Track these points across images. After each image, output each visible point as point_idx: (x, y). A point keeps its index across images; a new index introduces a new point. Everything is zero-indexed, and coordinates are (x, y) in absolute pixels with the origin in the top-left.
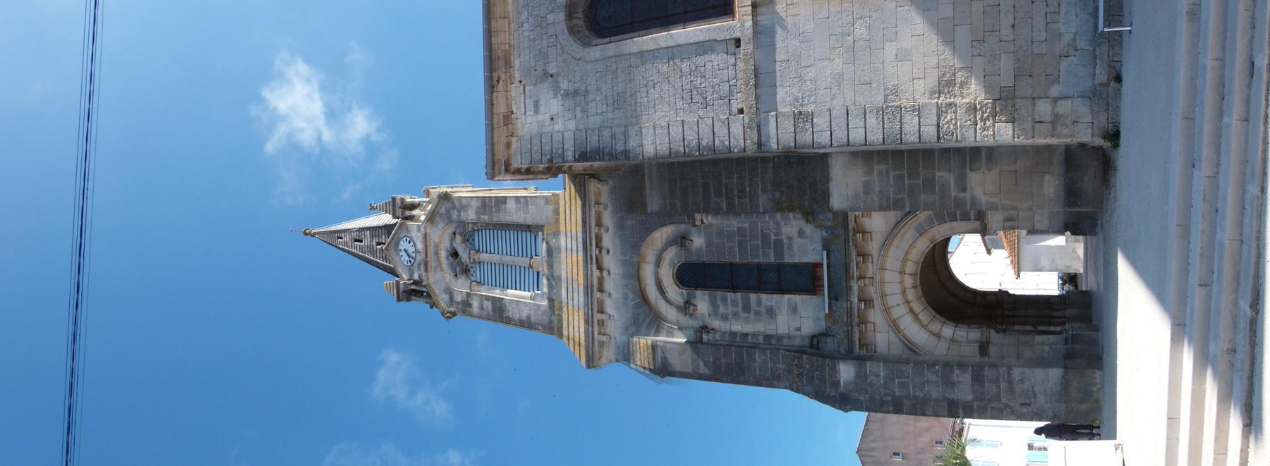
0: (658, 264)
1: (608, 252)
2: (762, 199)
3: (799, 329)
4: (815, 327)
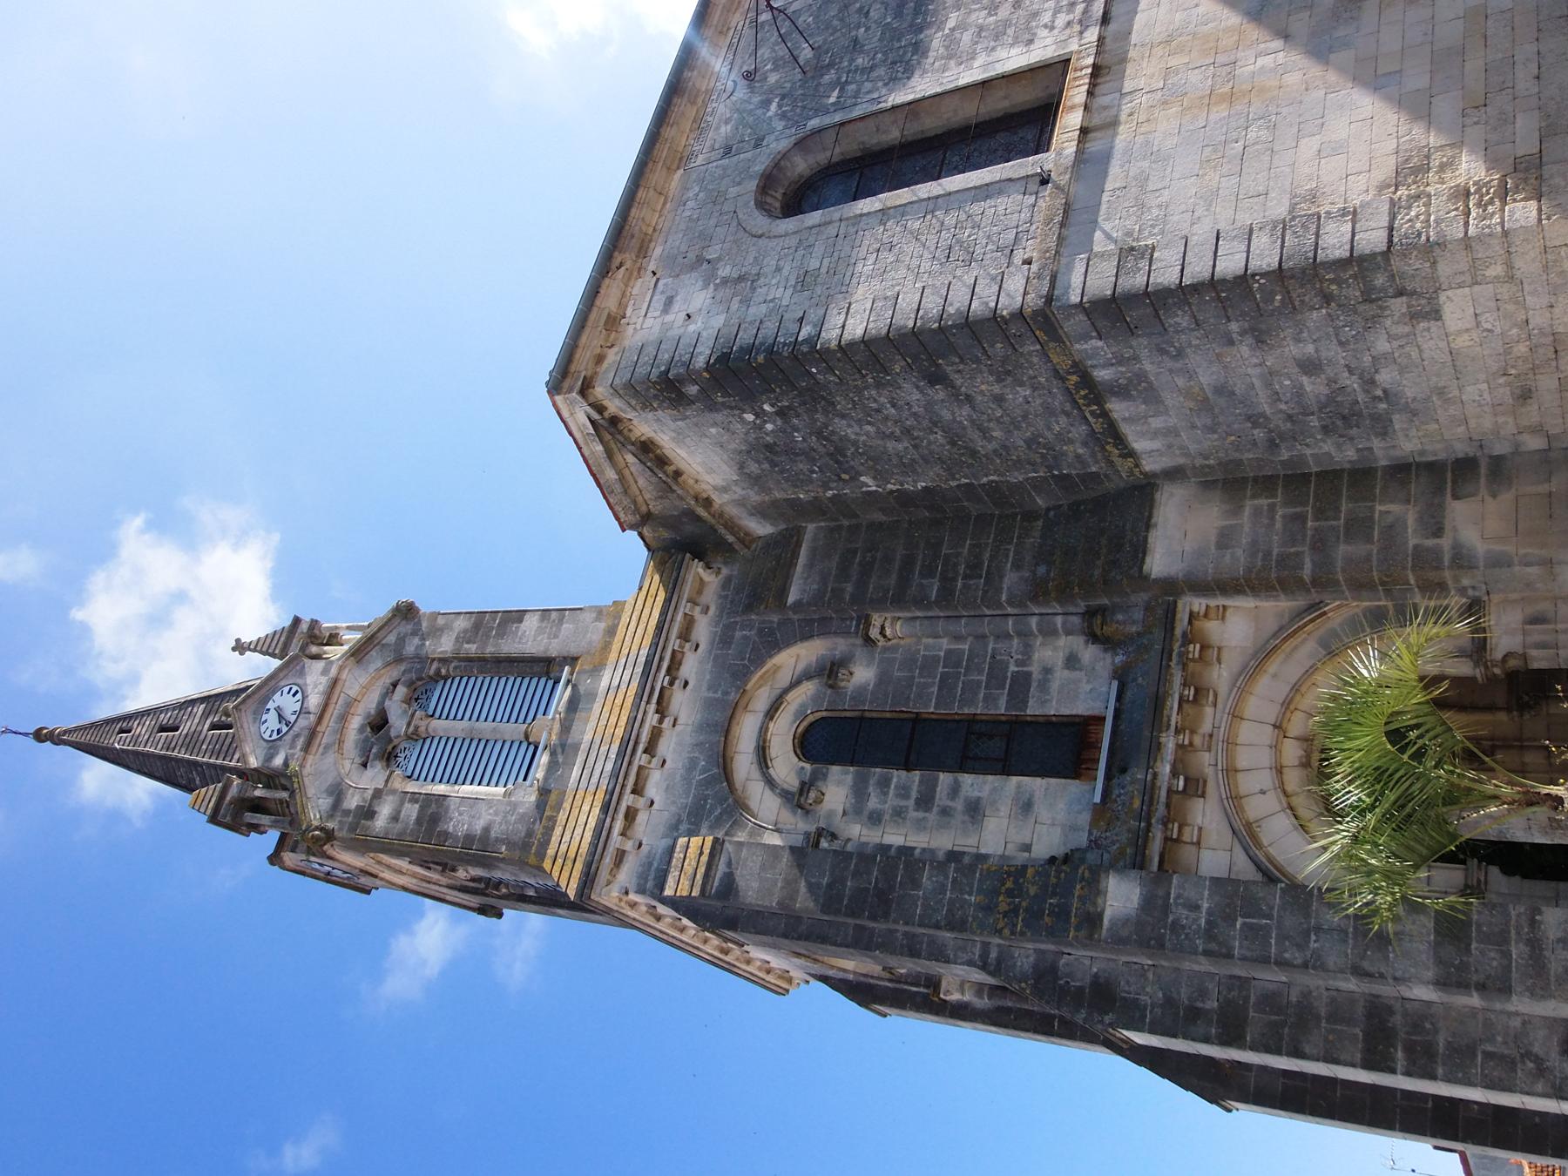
0: (771, 713)
1: (686, 684)
2: (1011, 580)
3: (1027, 848)
4: (1065, 844)
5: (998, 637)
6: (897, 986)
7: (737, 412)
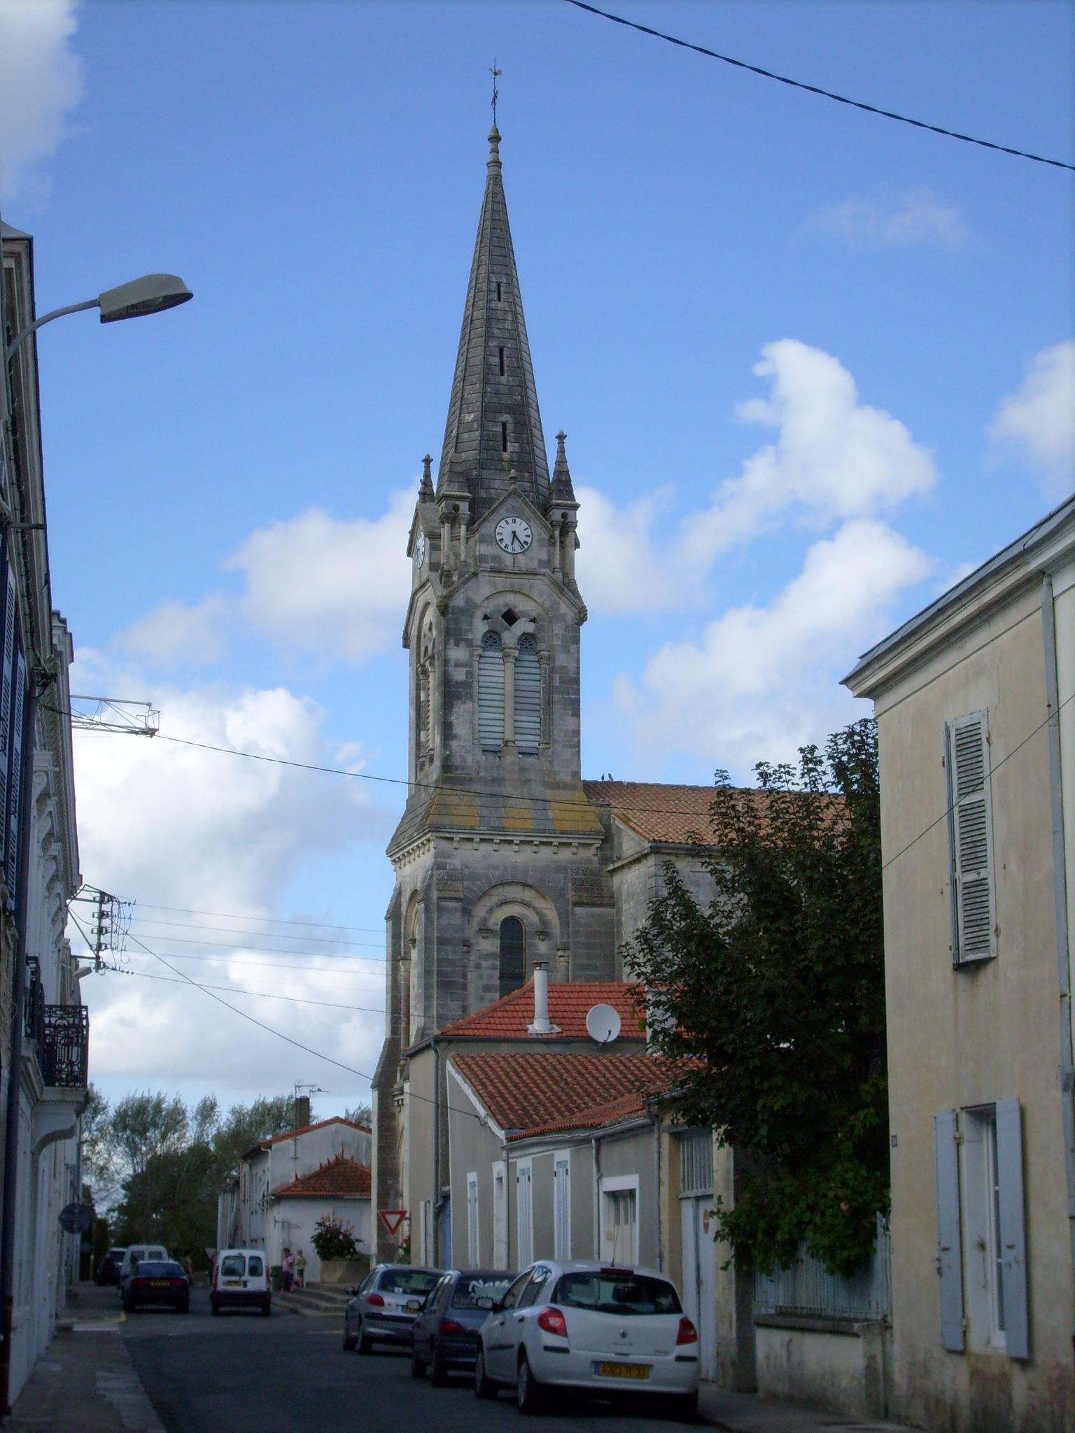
6: (402, 936)
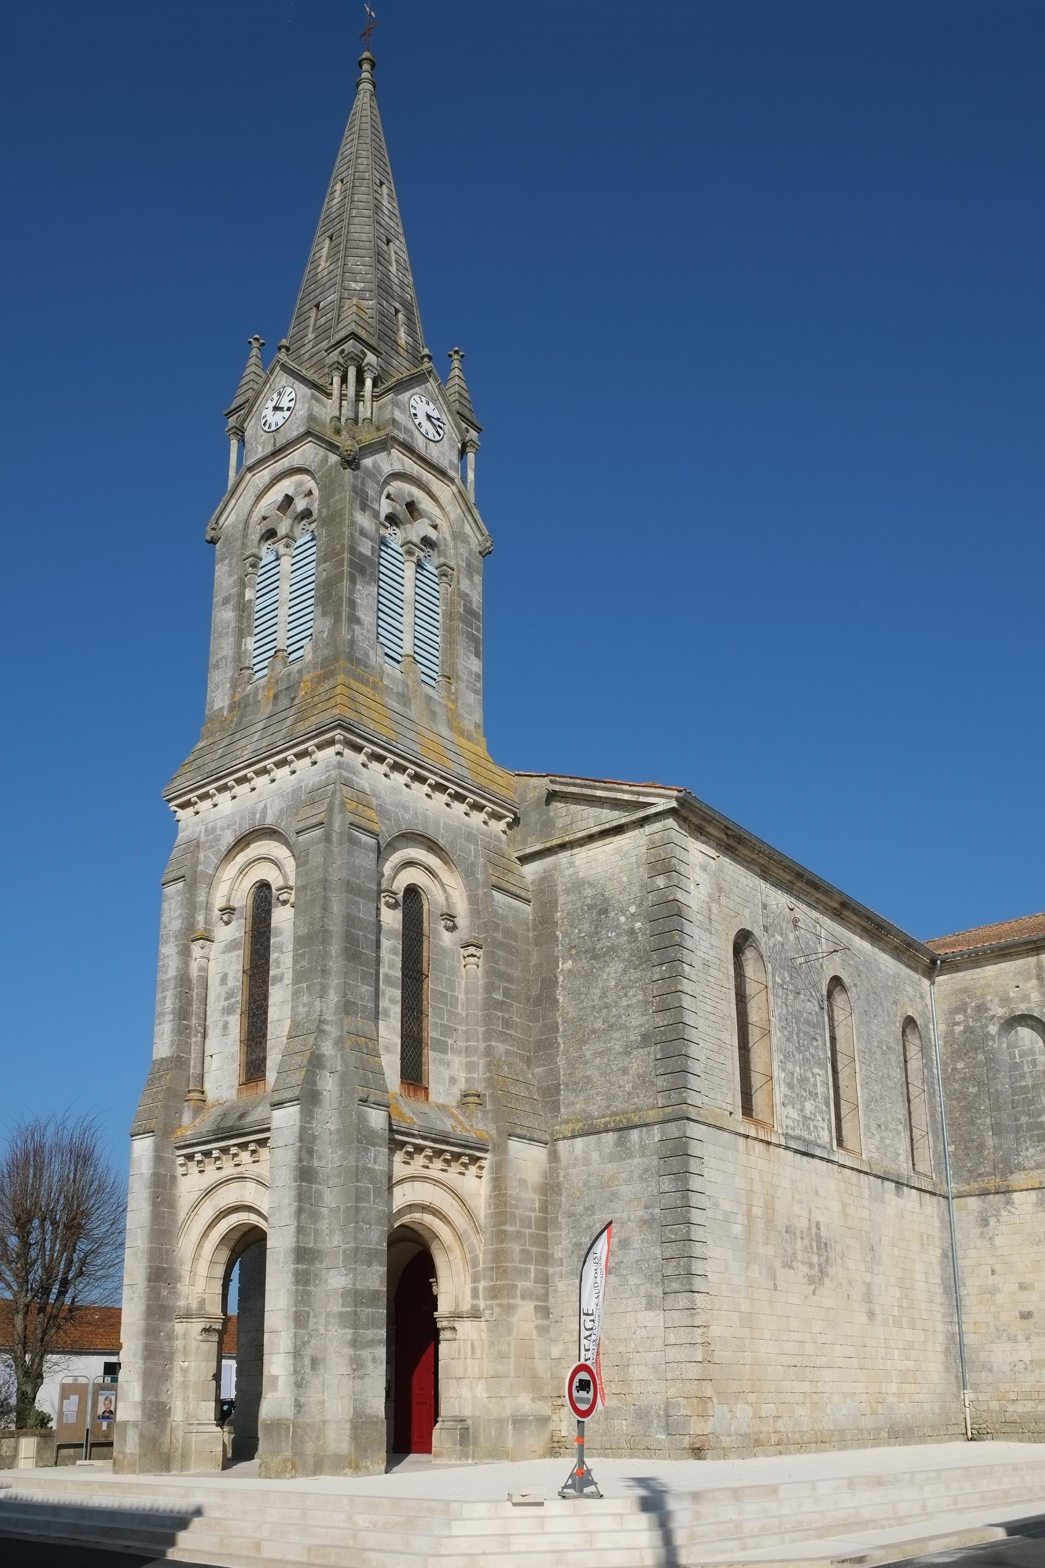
5: (466, 1032)
7: (638, 902)
